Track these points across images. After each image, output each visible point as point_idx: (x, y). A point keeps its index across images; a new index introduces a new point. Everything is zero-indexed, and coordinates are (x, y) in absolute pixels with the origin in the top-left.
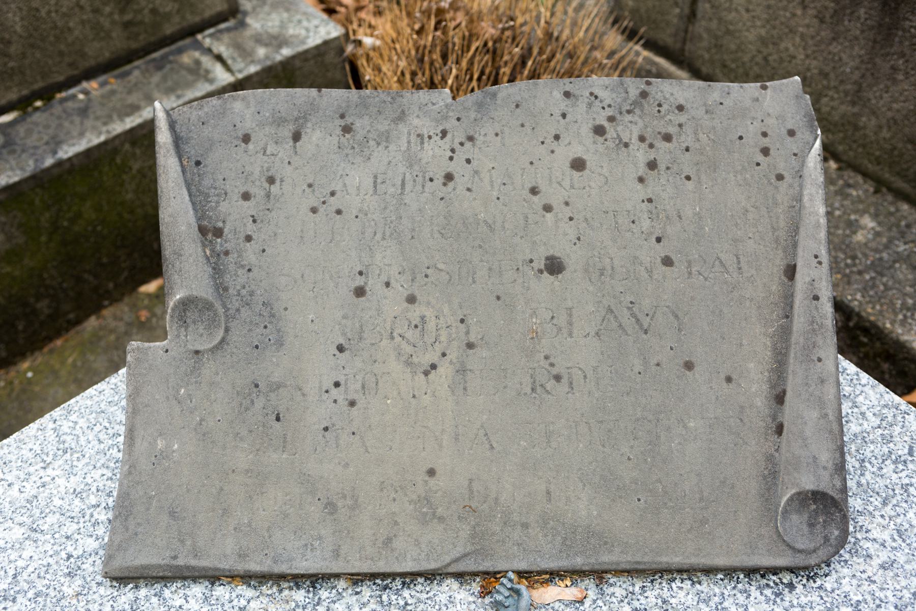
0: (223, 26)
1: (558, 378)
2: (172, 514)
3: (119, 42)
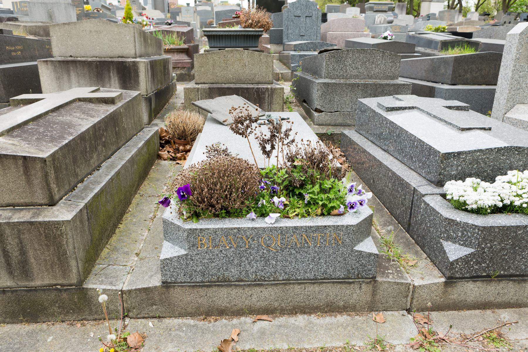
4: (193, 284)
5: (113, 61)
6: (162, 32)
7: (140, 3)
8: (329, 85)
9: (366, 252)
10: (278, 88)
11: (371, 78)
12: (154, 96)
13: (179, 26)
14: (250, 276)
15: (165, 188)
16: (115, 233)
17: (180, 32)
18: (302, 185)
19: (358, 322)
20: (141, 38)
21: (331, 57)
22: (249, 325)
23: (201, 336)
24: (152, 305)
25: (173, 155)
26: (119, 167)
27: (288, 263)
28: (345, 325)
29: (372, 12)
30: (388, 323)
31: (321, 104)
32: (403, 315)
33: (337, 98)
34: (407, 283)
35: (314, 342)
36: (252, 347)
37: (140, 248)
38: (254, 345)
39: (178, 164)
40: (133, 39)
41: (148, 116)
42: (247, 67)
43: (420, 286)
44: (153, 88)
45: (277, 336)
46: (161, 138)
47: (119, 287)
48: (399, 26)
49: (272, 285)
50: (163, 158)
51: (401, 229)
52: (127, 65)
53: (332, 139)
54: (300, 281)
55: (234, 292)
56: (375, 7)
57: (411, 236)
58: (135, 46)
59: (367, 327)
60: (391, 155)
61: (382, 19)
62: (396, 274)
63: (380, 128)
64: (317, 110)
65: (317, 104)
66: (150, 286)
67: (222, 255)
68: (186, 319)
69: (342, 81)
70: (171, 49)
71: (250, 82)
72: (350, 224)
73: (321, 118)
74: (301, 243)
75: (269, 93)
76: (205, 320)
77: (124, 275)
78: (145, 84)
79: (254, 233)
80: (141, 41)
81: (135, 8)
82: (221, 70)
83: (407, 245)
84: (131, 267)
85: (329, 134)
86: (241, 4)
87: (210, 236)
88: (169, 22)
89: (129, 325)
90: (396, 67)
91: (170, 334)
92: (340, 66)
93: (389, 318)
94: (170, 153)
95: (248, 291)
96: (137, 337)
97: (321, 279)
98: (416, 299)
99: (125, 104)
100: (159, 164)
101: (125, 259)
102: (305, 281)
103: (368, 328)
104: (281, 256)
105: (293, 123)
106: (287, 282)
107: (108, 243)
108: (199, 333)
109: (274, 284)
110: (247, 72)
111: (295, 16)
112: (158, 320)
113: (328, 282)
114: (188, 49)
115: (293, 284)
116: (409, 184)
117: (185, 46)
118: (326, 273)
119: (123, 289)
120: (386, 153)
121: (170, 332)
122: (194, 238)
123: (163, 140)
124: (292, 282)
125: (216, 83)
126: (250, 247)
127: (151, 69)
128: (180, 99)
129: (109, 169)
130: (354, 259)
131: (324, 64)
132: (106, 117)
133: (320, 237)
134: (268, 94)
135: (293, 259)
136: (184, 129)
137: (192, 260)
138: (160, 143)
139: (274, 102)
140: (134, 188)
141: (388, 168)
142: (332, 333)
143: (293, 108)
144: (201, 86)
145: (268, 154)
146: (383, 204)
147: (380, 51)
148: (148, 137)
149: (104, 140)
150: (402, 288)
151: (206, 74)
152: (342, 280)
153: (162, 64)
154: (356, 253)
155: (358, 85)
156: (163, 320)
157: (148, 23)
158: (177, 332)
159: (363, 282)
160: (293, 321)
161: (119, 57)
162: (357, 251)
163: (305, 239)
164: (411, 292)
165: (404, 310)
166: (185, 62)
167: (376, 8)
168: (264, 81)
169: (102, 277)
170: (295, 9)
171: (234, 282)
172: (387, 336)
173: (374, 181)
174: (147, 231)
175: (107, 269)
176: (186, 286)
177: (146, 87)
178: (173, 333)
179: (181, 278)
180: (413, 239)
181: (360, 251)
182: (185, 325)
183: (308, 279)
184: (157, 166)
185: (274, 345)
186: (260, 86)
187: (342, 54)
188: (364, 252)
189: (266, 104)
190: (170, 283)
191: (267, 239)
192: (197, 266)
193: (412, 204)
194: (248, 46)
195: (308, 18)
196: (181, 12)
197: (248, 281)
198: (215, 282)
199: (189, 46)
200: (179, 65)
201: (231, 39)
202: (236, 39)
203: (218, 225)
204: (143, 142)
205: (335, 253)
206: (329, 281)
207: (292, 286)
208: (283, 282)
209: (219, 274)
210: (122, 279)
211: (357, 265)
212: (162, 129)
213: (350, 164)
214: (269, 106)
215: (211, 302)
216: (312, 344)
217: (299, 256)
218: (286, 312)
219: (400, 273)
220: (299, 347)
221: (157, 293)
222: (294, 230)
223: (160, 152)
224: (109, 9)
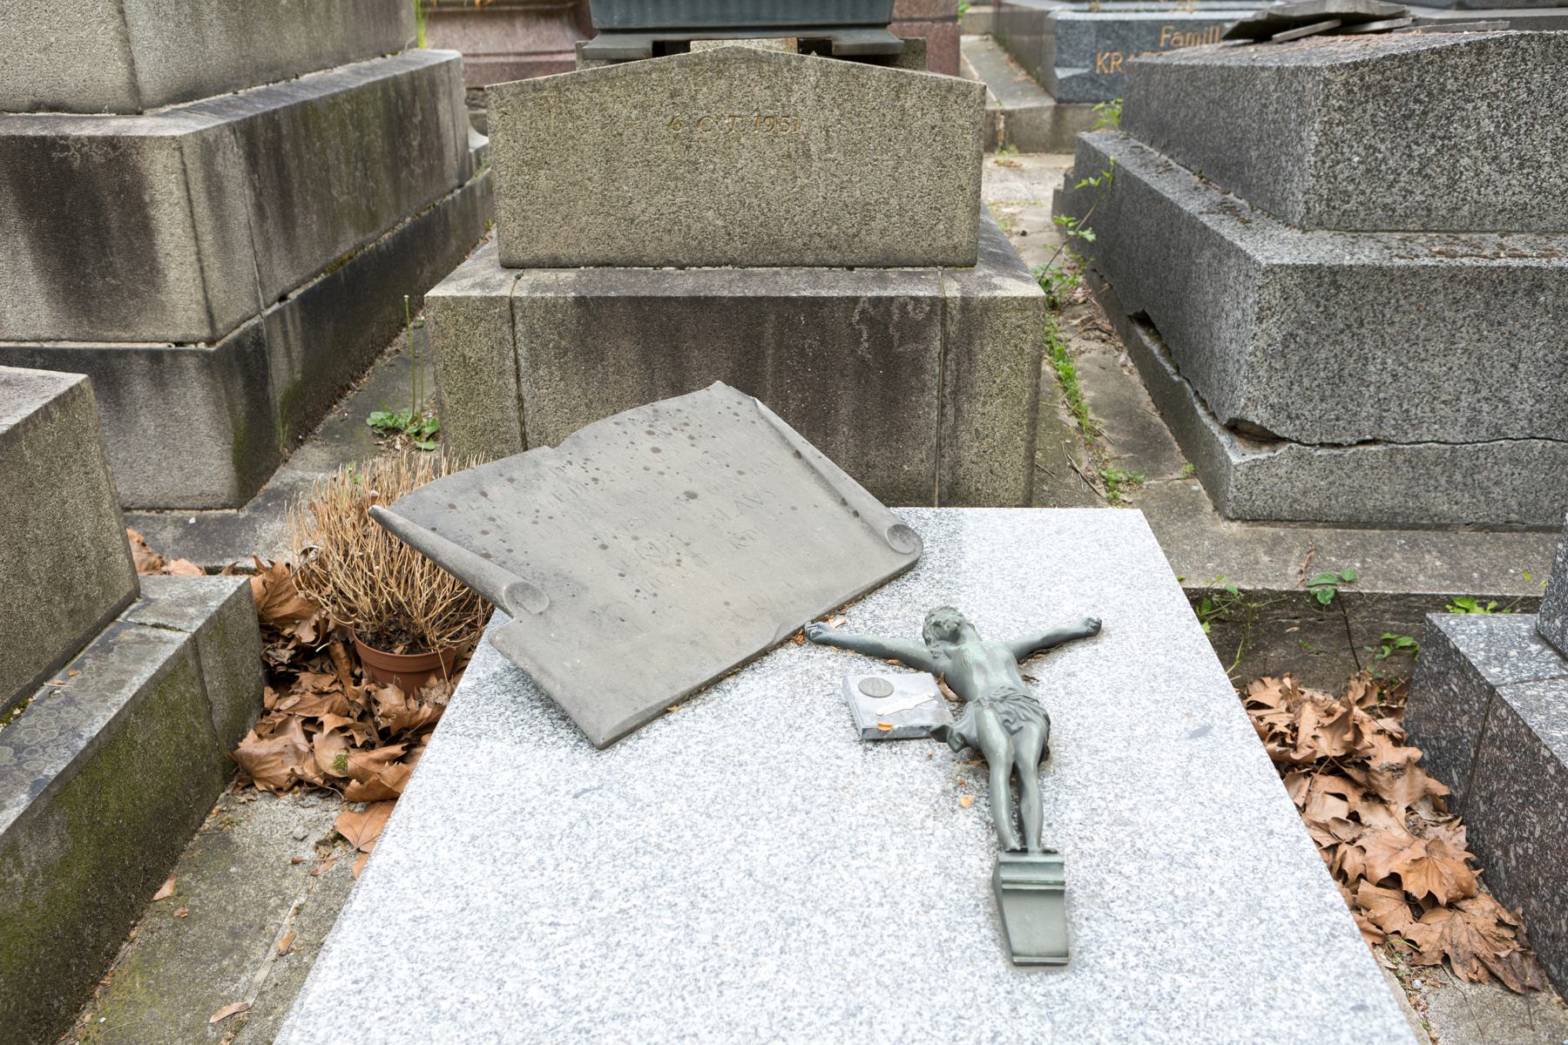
0: (133, 606)
1: (743, 538)
2: (613, 691)
3: (68, 635)
8: (1341, 280)
31: (1273, 399)
33: (1381, 364)
42: (817, 164)
46: (271, 630)
52: (76, 164)
53: (1339, 628)
64: (1236, 428)
69: (1425, 254)
73: (1268, 482)
75: (952, 329)
82: (655, 181)
85: (1325, 599)
92: (1418, 151)
110: (816, 195)
131: (1312, 139)
134: (946, 335)
139: (981, 387)
143: (1074, 346)
161: (35, 107)
168: (919, 250)
177: (200, 296)
186: (900, 287)
187: (1441, 72)
189: (932, 397)
194: (833, 21)
214: (950, 411)
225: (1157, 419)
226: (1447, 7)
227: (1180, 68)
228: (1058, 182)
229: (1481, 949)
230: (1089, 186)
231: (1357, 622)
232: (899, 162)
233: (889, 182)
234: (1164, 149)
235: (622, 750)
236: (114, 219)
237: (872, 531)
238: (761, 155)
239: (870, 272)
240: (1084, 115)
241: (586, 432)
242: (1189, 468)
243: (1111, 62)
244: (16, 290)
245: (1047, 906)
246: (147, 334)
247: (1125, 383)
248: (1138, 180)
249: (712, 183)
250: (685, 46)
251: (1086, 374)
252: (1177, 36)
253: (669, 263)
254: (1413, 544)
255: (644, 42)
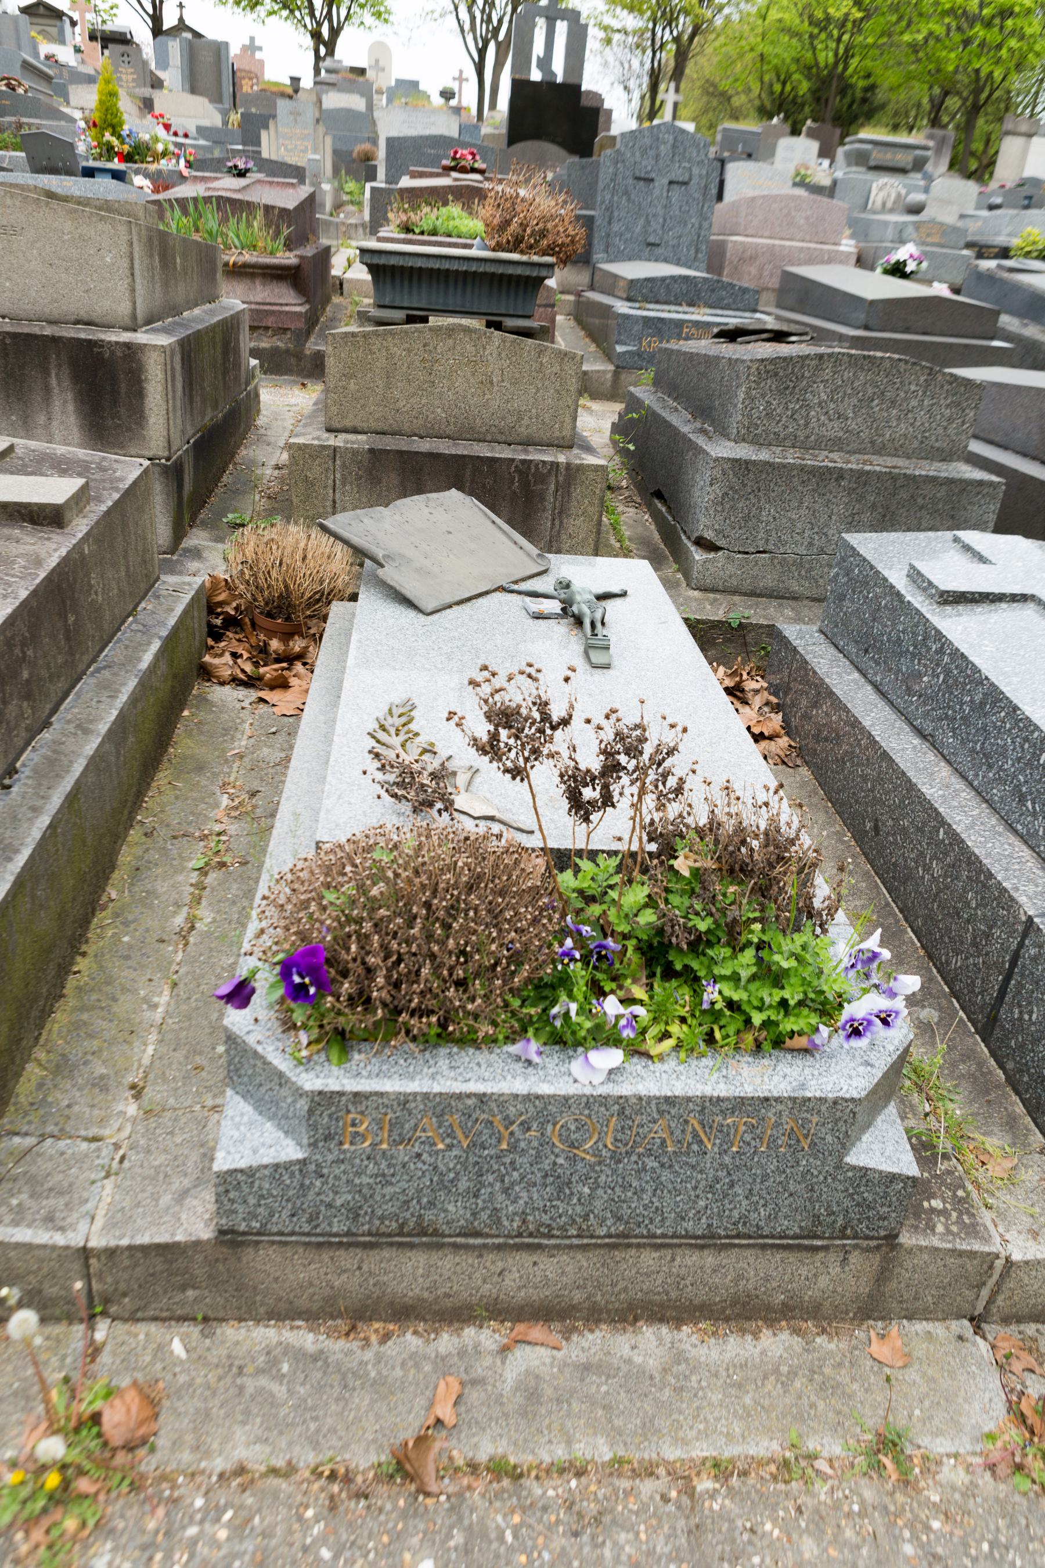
4: (321, 1239)
5: (60, 338)
6: (218, 204)
7: (145, 63)
9: (881, 1172)
10: (589, 466)
11: (880, 450)
12: (191, 454)
13: (271, 183)
14: (506, 1223)
15: (225, 801)
16: (63, 996)
17: (273, 207)
18: (698, 944)
19: (825, 1360)
20: (151, 256)
21: (764, 376)
22: (488, 1361)
23: (337, 1400)
24: (184, 1288)
25: (248, 668)
26: (78, 768)
27: (629, 1194)
28: (784, 1369)
29: (862, 169)
30: (916, 1366)
31: (717, 527)
32: (960, 1338)
33: (768, 512)
34: (989, 1254)
35: (691, 1434)
36: (500, 1451)
37: (146, 1061)
38: (504, 1442)
39: (266, 702)
40: (125, 263)
41: (170, 524)
42: (496, 388)
43: (1027, 1263)
44: (188, 427)
45: (576, 1406)
46: (211, 609)
47: (74, 1239)
48: (942, 224)
49: (571, 1247)
50: (217, 677)
51: (961, 1019)
52: (107, 356)
53: (741, 641)
54: (659, 1241)
55: (447, 1263)
56: (874, 155)
57: (993, 1054)
58: (133, 290)
59: (853, 1379)
60: (943, 756)
61: (889, 195)
62: (954, 1214)
63: (913, 655)
64: (702, 543)
65: (705, 525)
66: (179, 1237)
67: (420, 1165)
68: (292, 1328)
69: (791, 457)
70: (245, 265)
71: (502, 438)
72: (847, 1096)
73: (712, 570)
74: (679, 1142)
75: (561, 479)
76: (352, 1336)
77: (93, 1182)
78: (162, 420)
79: (532, 1109)
80: (151, 268)
81: (131, 77)
83: (982, 1087)
84: (117, 1146)
85: (735, 625)
86: (456, 90)
87: (386, 1114)
88: (241, 165)
89: (108, 1348)
90: (963, 423)
91: (241, 1389)
92: (791, 406)
93: (920, 1349)
94: (239, 661)
95: (493, 1262)
96: (134, 1409)
97: (727, 1237)
98: (1008, 1293)
99: (97, 523)
100: (203, 699)
101: (96, 1112)
102: (675, 1241)
103: (855, 1386)
104: (609, 1173)
105: (685, 730)
106: (621, 1241)
107: (42, 1041)
108: (332, 1387)
109: (578, 1246)
110: (495, 404)
111: (638, 179)
112: (200, 1327)
113: (749, 1246)
114: (297, 268)
115: (639, 1246)
116: (1012, 899)
117: (288, 258)
118: (745, 1224)
119: (90, 1244)
120: (925, 746)
121: (239, 1381)
122: (330, 1116)
123: (219, 614)
124: (634, 1241)
125: (394, 434)
126: (513, 1148)
127: (183, 368)
128: (269, 449)
129: (45, 783)
130: (841, 1187)
132: (34, 593)
133: (743, 1128)
134: (557, 481)
135: (647, 1182)
136: (286, 587)
137: (322, 1176)
138: (210, 626)
139: (573, 511)
140: (126, 812)
141: (938, 813)
142: (748, 1400)
144: (346, 442)
145: (580, 808)
146: (901, 911)
147: (923, 367)
148: (172, 621)
149: (25, 675)
150: (970, 1266)
151: (362, 402)
152: (791, 1242)
153: (218, 338)
154: (850, 1174)
155: (840, 474)
156: (219, 1331)
157: (171, 148)
158: (263, 1381)
159: (856, 1247)
160: (626, 1351)
161: (77, 322)
162: (854, 1168)
163: (694, 1129)
164: (995, 1277)
165: (965, 1317)
166: (287, 313)
167: (878, 156)
168: (545, 437)
169: (19, 1192)
170: (638, 154)
171: (450, 1236)
172: (915, 1420)
173: (876, 829)
174: (167, 992)
175: (39, 1155)
176: (297, 1242)
178: (251, 1385)
179: (281, 1221)
180: (1001, 1066)
181: (861, 1169)
182: (287, 1349)
183: (687, 1236)
184: (198, 708)
185: (569, 1443)
186: (535, 455)
187: (802, 367)
188: (875, 1171)
190: (244, 1233)
191: (573, 1128)
192: (336, 1193)
193: (1014, 963)
194: (503, 312)
195: (675, 186)
196: (274, 117)
197: (497, 1236)
198: (390, 1235)
199: (301, 257)
200: (269, 322)
201: (447, 282)
202: (465, 283)
203: (412, 1079)
204: (156, 645)
205: (784, 1172)
206: (751, 1241)
207: (633, 1252)
208: (607, 1240)
209: (408, 1215)
210: (87, 1201)
211: (847, 1203)
212: (214, 580)
213: (794, 740)
214: (557, 522)
215: (375, 1285)
216: (685, 1442)
217: (666, 1176)
218: (604, 1316)
219: (968, 1213)
220: (647, 1457)
221: (199, 1258)
222: (665, 1107)
223: (207, 658)
224: (48, 78)
225: (662, 546)
226: (858, 328)
227: (685, 353)
228: (615, 418)
229: (782, 754)
230: (632, 418)
231: (750, 638)
232: (538, 391)
233: (532, 400)
234: (675, 399)
235: (436, 616)
236: (123, 388)
237: (529, 555)
238: (468, 381)
239: (520, 447)
240: (632, 378)
241: (399, 502)
242: (675, 566)
243: (652, 344)
244: (62, 423)
245: (603, 652)
246: (133, 453)
247: (647, 529)
248: (659, 415)
249: (441, 394)
250: (425, 320)
251: (626, 523)
252: (693, 331)
253: (415, 435)
254: (780, 605)
255: (401, 315)
